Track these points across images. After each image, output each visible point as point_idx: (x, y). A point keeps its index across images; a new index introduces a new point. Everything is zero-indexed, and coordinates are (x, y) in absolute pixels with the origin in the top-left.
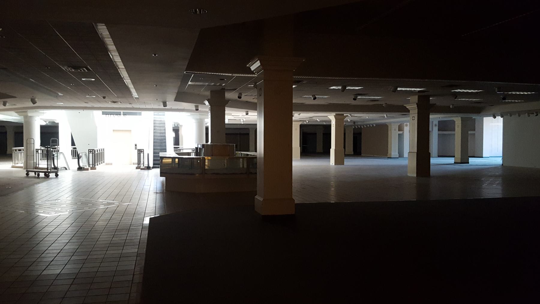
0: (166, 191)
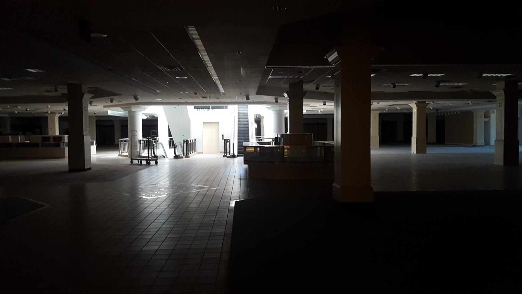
0: (249, 177)
